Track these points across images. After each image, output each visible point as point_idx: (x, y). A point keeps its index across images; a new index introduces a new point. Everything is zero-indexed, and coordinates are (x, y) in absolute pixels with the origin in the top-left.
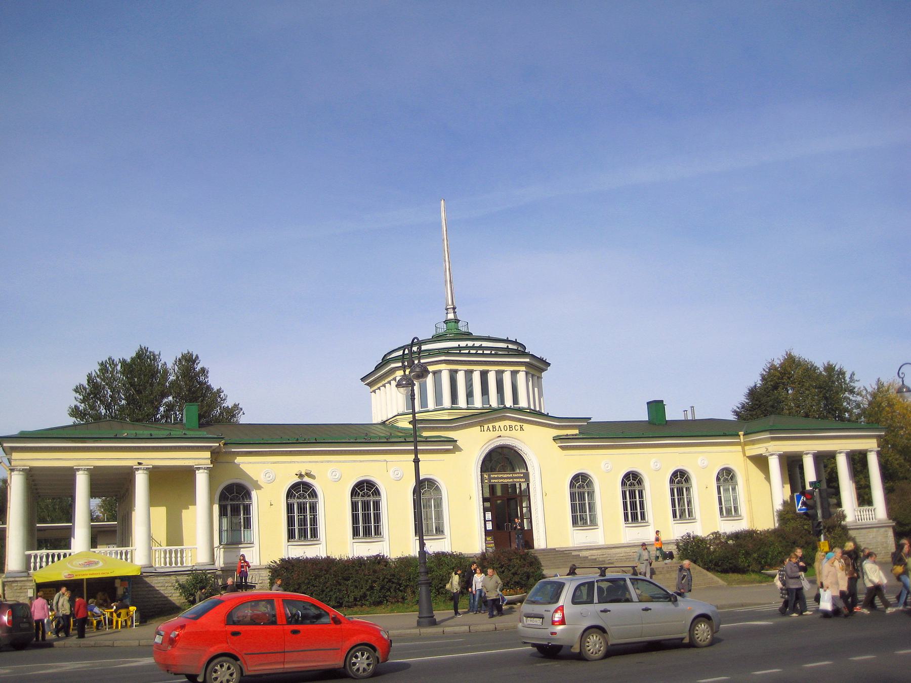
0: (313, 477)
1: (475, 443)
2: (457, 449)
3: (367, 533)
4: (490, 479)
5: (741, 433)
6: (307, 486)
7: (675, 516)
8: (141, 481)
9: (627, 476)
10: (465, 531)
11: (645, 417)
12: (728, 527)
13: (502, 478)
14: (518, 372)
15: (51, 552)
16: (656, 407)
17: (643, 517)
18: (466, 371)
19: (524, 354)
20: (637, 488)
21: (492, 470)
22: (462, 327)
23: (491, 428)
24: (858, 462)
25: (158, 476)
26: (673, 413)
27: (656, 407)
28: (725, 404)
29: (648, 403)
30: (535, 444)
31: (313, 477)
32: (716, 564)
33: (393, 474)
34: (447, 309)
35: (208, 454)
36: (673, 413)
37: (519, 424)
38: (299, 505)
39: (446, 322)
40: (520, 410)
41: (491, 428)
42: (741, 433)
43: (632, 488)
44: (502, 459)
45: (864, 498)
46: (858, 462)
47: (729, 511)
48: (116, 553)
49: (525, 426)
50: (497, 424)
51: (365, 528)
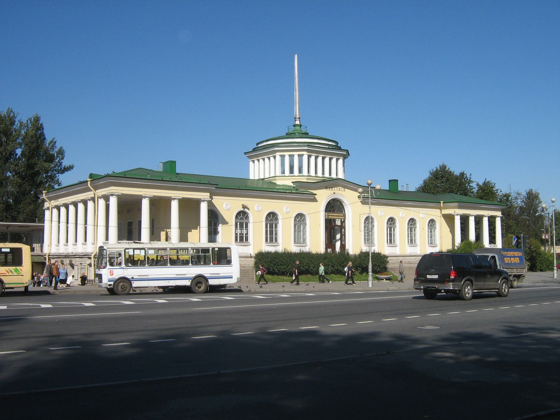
0: (248, 209)
1: (324, 196)
2: (315, 200)
3: (271, 240)
4: (328, 216)
5: (442, 202)
7: (236, 240)
8: (175, 206)
9: (239, 214)
10: (315, 243)
11: (387, 188)
12: (294, 249)
14: (303, 155)
16: (393, 183)
17: (276, 240)
19: (339, 149)
20: (245, 221)
21: (330, 211)
24: (492, 220)
25: (183, 202)
26: (179, 169)
27: (393, 183)
28: (412, 182)
29: (389, 181)
30: (350, 199)
31: (248, 209)
33: (286, 210)
34: (295, 118)
36: (179, 169)
42: (442, 202)
43: (271, 222)
44: (335, 206)
45: (492, 240)
46: (492, 220)
47: (432, 243)
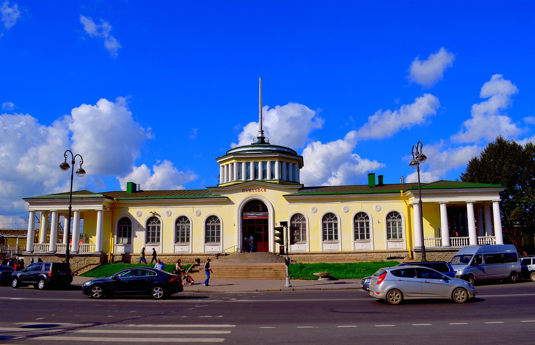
1: (239, 198)
3: (183, 240)
13: (252, 215)
18: (263, 162)
51: (361, 235)
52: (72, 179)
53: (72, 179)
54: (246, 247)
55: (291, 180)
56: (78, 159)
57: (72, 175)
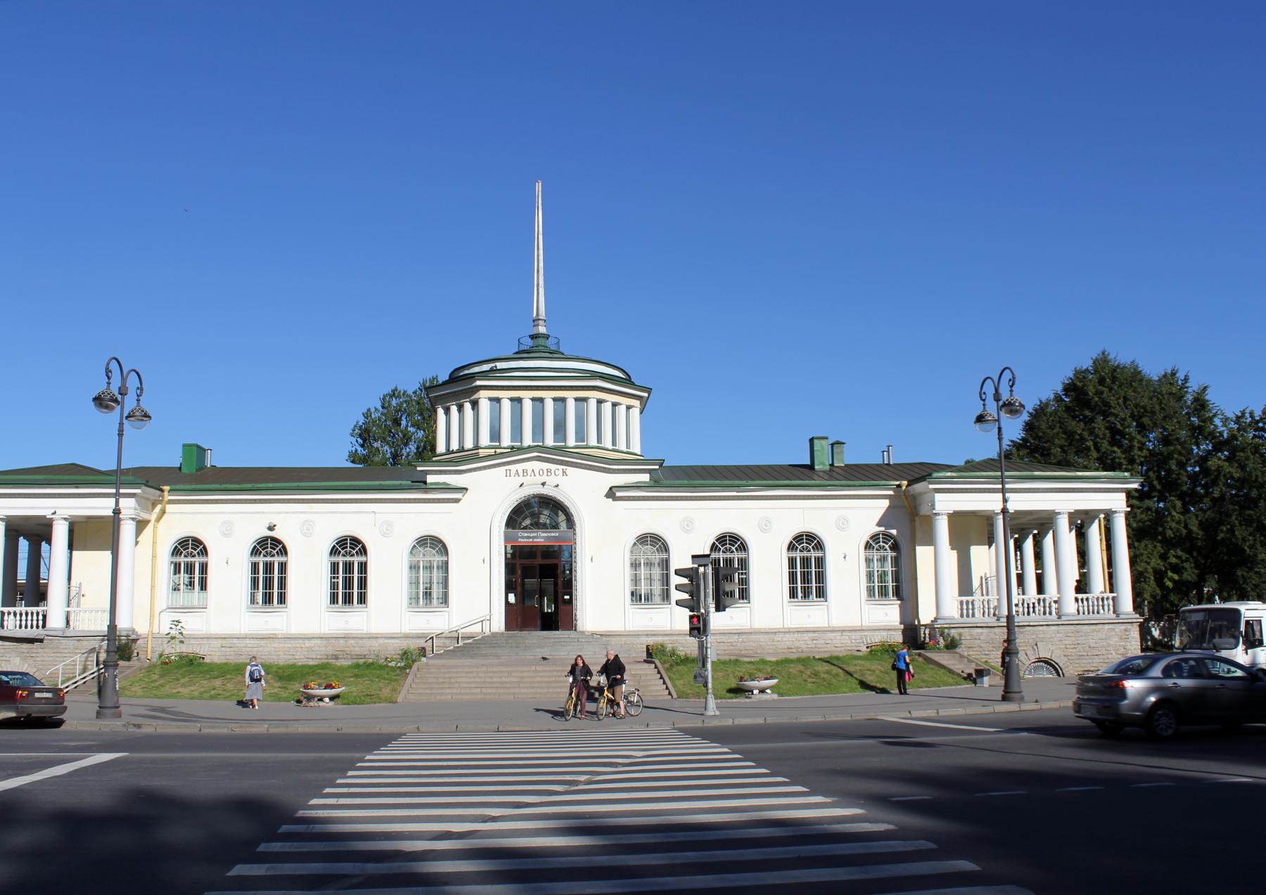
3: (348, 600)
6: (276, 542)
13: (540, 538)
15: (30, 609)
22: (551, 343)
23: (521, 473)
26: (215, 459)
29: (184, 446)
32: (207, 672)
35: (1123, 495)
37: (561, 467)
38: (345, 564)
39: (533, 337)
40: (521, 450)
41: (521, 473)
48: (15, 614)
49: (570, 470)
50: (513, 467)
51: (804, 589)
52: (121, 434)
53: (121, 434)
54: (519, 617)
55: (624, 448)
56: (132, 382)
57: (121, 424)
